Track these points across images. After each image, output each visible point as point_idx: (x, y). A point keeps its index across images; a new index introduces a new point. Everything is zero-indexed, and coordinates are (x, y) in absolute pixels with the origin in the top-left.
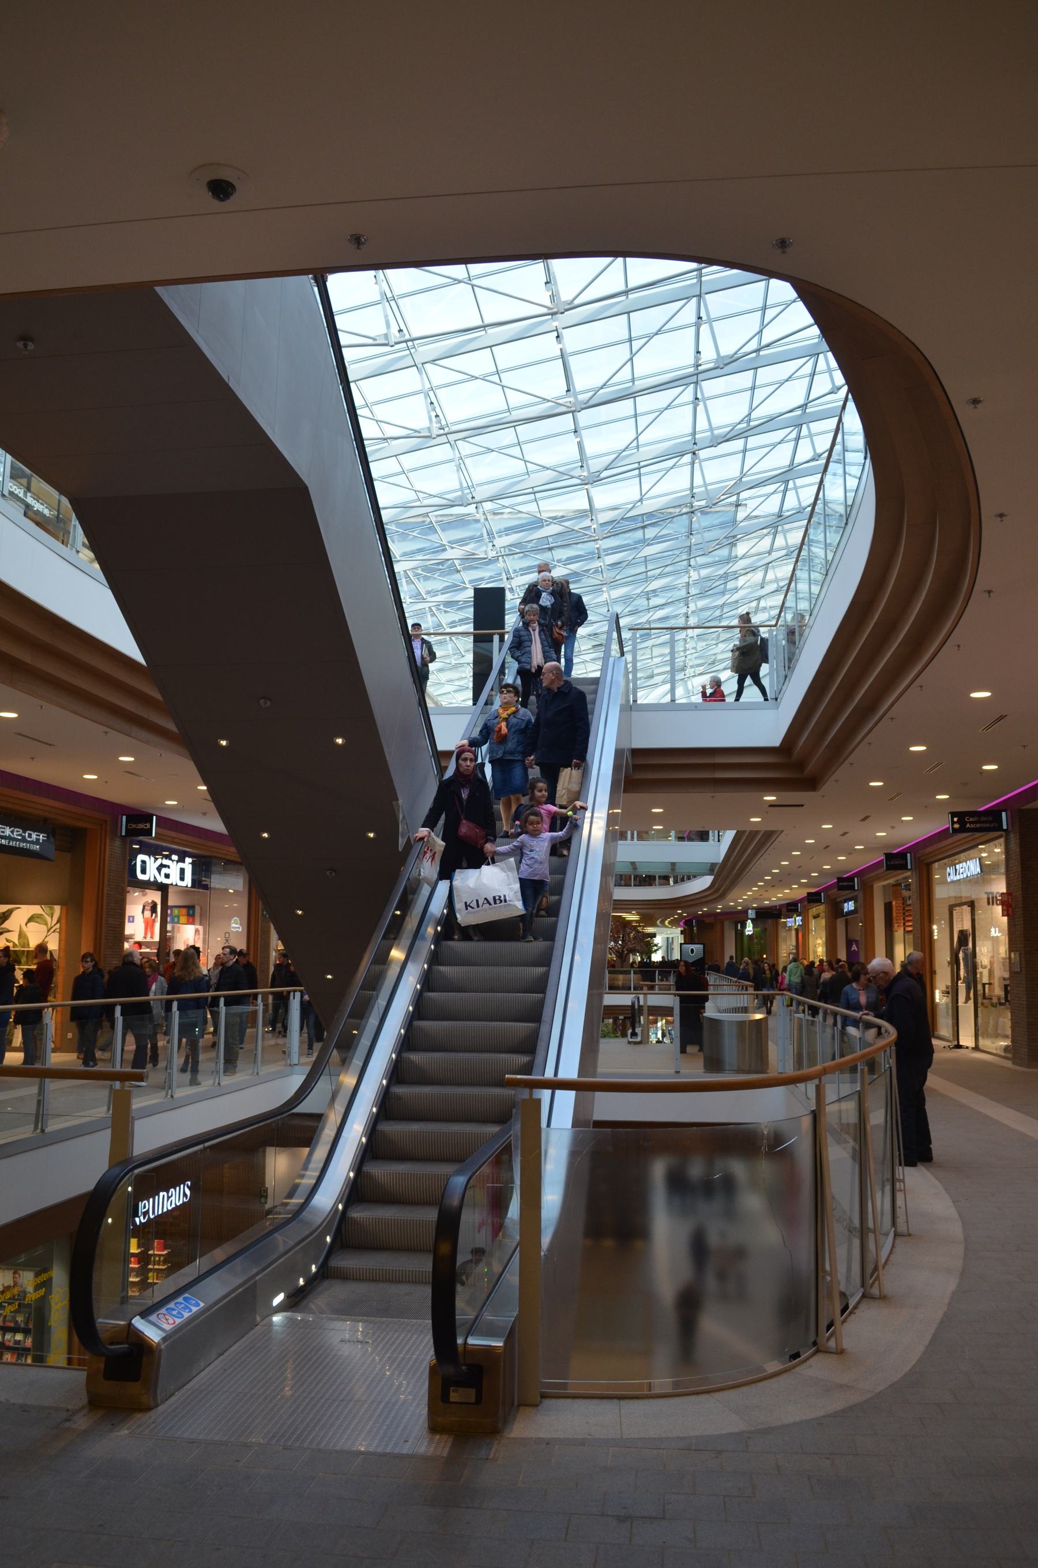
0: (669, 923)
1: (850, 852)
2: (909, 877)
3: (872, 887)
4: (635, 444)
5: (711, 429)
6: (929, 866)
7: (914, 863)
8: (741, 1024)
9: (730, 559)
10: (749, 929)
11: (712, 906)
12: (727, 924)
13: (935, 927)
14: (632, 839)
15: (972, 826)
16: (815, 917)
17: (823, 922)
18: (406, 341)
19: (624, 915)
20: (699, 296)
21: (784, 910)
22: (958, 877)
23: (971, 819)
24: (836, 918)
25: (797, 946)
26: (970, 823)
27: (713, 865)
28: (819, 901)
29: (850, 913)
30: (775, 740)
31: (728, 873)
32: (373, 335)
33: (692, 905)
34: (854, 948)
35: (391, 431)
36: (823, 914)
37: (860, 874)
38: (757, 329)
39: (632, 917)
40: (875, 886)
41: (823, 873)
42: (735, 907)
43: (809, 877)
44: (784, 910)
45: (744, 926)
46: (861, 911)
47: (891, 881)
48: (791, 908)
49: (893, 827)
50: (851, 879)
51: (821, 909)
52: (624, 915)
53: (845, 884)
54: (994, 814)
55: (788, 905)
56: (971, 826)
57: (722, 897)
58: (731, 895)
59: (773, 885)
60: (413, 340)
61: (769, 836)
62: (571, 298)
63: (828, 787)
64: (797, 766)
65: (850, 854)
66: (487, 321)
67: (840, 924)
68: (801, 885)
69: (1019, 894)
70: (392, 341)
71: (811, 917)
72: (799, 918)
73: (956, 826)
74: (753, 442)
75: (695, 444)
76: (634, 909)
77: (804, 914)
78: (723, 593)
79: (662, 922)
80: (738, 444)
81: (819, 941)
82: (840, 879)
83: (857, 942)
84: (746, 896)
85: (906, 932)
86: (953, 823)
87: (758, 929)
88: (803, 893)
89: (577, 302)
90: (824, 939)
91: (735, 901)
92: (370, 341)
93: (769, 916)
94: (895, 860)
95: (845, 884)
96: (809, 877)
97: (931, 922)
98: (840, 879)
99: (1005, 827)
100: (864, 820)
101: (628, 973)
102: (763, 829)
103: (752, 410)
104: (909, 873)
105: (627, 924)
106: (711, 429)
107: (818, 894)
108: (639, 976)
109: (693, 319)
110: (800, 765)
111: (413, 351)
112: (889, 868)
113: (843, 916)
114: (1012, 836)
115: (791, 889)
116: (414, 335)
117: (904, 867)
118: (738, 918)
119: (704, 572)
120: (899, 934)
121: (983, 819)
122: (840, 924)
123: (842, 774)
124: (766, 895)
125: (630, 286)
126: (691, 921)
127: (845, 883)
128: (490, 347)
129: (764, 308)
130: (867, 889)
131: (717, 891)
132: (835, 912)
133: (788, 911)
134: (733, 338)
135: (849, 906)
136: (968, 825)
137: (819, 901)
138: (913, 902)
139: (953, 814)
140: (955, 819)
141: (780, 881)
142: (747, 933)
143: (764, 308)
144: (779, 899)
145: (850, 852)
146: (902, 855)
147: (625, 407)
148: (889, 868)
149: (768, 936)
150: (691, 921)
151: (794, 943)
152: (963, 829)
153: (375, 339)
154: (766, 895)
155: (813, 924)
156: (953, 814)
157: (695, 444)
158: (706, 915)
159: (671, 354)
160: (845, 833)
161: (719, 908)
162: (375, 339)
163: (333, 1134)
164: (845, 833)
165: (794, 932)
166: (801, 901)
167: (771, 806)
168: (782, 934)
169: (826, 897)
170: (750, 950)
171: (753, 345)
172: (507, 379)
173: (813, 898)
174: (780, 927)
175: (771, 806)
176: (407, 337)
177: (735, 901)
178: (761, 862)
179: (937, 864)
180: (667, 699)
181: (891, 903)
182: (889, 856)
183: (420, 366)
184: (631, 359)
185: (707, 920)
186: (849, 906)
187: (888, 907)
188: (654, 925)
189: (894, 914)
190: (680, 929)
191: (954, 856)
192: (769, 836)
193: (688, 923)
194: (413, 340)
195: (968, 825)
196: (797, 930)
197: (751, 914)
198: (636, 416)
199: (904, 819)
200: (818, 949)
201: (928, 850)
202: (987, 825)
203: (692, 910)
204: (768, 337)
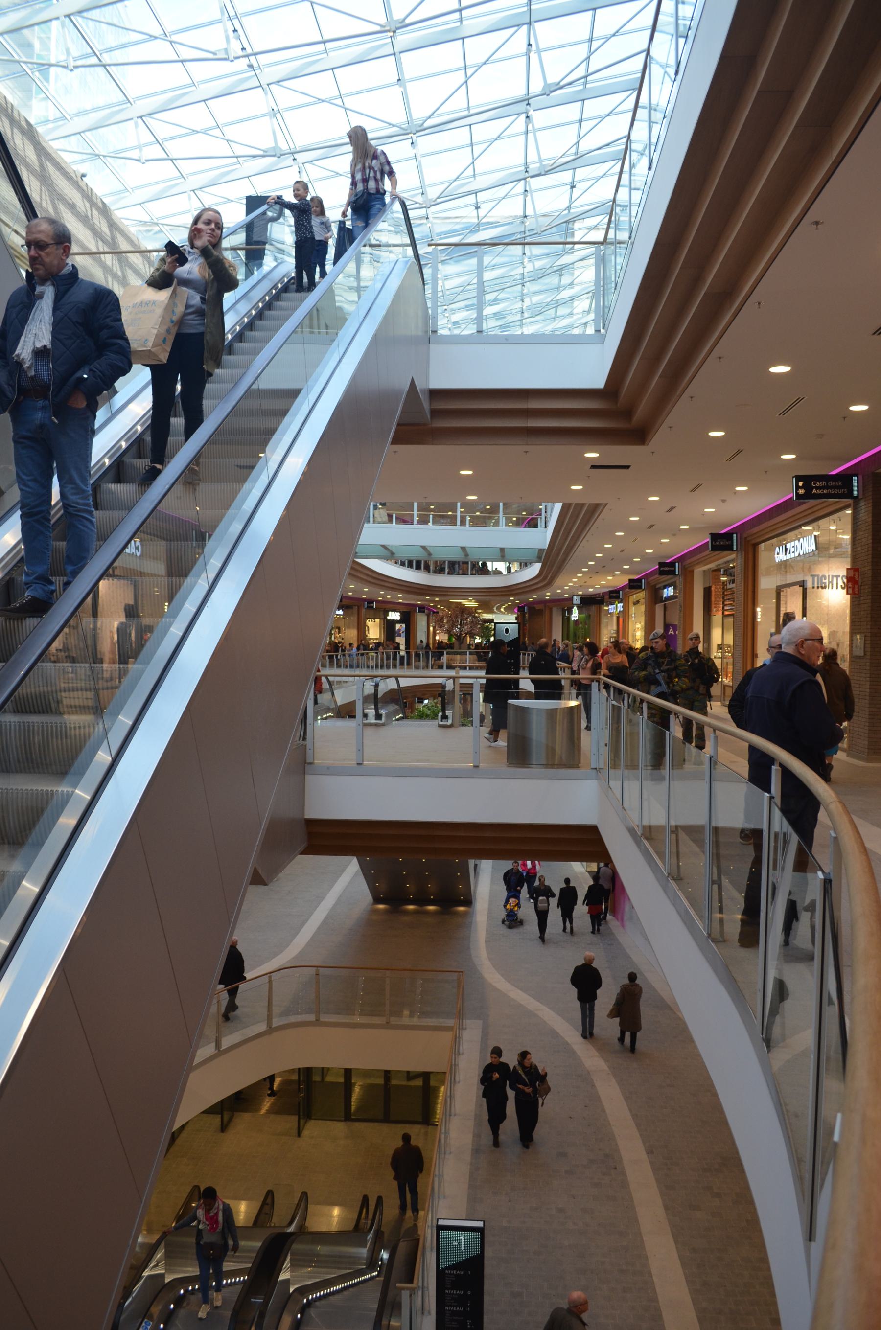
0: (505, 609)
1: (675, 533)
2: (732, 559)
3: (692, 571)
4: (470, 172)
5: (540, 160)
6: (755, 546)
7: (738, 544)
8: (552, 713)
9: (558, 288)
10: (575, 615)
11: (540, 593)
12: (555, 610)
13: (758, 610)
14: (463, 523)
15: (819, 492)
16: (635, 604)
17: (642, 608)
18: (248, 56)
19: (463, 602)
20: (530, 24)
21: (607, 597)
22: (788, 557)
23: (818, 484)
24: (656, 604)
25: (618, 631)
26: (817, 488)
27: (541, 550)
28: (640, 587)
29: (669, 598)
30: (597, 379)
31: (554, 560)
32: (213, 50)
33: (523, 592)
34: (671, 632)
35: (240, 150)
36: (643, 601)
37: (681, 559)
38: (585, 56)
39: (471, 604)
40: (695, 571)
41: (645, 558)
42: (562, 594)
43: (631, 563)
44: (607, 597)
45: (570, 612)
46: (680, 600)
47: (712, 566)
48: (614, 595)
49: (724, 501)
50: (672, 564)
51: (641, 595)
52: (463, 602)
53: (666, 569)
54: (845, 478)
55: (611, 592)
56: (818, 491)
57: (550, 584)
58: (559, 581)
59: (596, 571)
60: (255, 54)
61: (595, 509)
62: (402, 17)
63: (660, 438)
64: (621, 413)
65: (674, 535)
66: (326, 38)
67: (659, 609)
68: (624, 572)
69: (867, 569)
70: (232, 55)
71: (631, 604)
72: (620, 605)
73: (801, 491)
74: (581, 173)
75: (527, 171)
76: (470, 596)
77: (624, 601)
78: (555, 318)
79: (499, 609)
80: (566, 176)
81: (638, 626)
82: (661, 564)
83: (675, 628)
84: (572, 583)
85: (724, 616)
86: (798, 487)
87: (583, 615)
88: (623, 581)
89: (408, 21)
90: (643, 623)
91: (562, 588)
92: (211, 56)
93: (592, 603)
94: (721, 541)
95: (666, 569)
96: (631, 563)
97: (754, 605)
98: (661, 564)
99: (855, 494)
100: (693, 490)
101: (465, 653)
102: (589, 500)
103: (580, 137)
104: (733, 556)
105: (463, 610)
106: (540, 160)
107: (639, 580)
108: (475, 657)
109: (524, 49)
110: (628, 413)
111: (258, 72)
112: (714, 548)
113: (662, 601)
114: (862, 503)
115: (614, 576)
116: (256, 50)
117: (729, 548)
118: (565, 605)
119: (536, 299)
120: (717, 618)
121: (831, 484)
122: (659, 609)
123: (679, 414)
124: (590, 582)
125: (463, 5)
126: (523, 607)
127: (666, 569)
128: (332, 69)
129: (591, 40)
130: (688, 574)
131: (546, 578)
132: (655, 597)
133: (611, 597)
134: (558, 66)
135: (669, 592)
136: (814, 491)
137: (640, 587)
138: (737, 586)
139: (799, 478)
140: (801, 484)
141: (603, 568)
142: (573, 619)
143: (591, 40)
144: (602, 586)
145: (675, 533)
146: (728, 536)
147: (460, 136)
148: (714, 548)
149: (592, 623)
150: (523, 607)
151: (615, 628)
152: (808, 495)
153: (214, 54)
154: (590, 582)
155: (633, 609)
156: (799, 478)
157: (527, 171)
158: (536, 602)
159: (504, 82)
160: (672, 509)
161: (548, 595)
162: (214, 54)
163: (73, 822)
164: (672, 509)
165: (615, 618)
166: (623, 588)
167: (593, 467)
168: (604, 621)
169: (647, 583)
170: (575, 634)
171: (581, 72)
172: (349, 102)
173: (634, 585)
174: (602, 614)
175: (593, 467)
176: (249, 51)
177: (562, 588)
178: (585, 545)
179: (763, 544)
180: (471, 330)
181: (710, 588)
182: (715, 537)
183: (265, 86)
184: (466, 82)
185: (538, 607)
186: (669, 592)
187: (707, 592)
188: (492, 612)
189: (713, 599)
190: (515, 615)
191: (792, 527)
192: (595, 509)
193: (521, 609)
194: (255, 54)
195: (814, 491)
196: (618, 618)
197: (576, 600)
198: (472, 145)
199: (738, 489)
200: (637, 637)
201: (755, 530)
202: (836, 491)
203: (523, 597)
204: (594, 66)
